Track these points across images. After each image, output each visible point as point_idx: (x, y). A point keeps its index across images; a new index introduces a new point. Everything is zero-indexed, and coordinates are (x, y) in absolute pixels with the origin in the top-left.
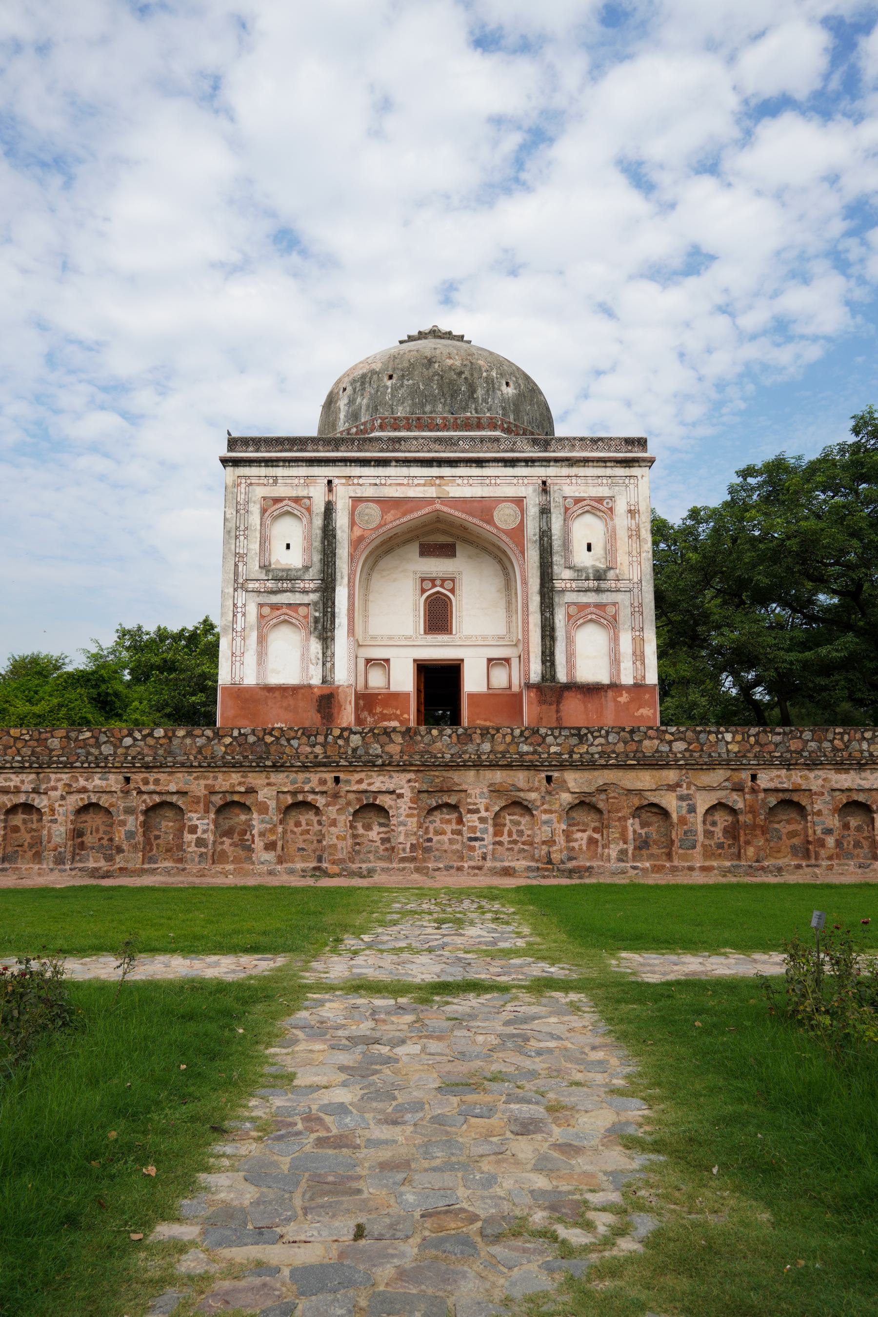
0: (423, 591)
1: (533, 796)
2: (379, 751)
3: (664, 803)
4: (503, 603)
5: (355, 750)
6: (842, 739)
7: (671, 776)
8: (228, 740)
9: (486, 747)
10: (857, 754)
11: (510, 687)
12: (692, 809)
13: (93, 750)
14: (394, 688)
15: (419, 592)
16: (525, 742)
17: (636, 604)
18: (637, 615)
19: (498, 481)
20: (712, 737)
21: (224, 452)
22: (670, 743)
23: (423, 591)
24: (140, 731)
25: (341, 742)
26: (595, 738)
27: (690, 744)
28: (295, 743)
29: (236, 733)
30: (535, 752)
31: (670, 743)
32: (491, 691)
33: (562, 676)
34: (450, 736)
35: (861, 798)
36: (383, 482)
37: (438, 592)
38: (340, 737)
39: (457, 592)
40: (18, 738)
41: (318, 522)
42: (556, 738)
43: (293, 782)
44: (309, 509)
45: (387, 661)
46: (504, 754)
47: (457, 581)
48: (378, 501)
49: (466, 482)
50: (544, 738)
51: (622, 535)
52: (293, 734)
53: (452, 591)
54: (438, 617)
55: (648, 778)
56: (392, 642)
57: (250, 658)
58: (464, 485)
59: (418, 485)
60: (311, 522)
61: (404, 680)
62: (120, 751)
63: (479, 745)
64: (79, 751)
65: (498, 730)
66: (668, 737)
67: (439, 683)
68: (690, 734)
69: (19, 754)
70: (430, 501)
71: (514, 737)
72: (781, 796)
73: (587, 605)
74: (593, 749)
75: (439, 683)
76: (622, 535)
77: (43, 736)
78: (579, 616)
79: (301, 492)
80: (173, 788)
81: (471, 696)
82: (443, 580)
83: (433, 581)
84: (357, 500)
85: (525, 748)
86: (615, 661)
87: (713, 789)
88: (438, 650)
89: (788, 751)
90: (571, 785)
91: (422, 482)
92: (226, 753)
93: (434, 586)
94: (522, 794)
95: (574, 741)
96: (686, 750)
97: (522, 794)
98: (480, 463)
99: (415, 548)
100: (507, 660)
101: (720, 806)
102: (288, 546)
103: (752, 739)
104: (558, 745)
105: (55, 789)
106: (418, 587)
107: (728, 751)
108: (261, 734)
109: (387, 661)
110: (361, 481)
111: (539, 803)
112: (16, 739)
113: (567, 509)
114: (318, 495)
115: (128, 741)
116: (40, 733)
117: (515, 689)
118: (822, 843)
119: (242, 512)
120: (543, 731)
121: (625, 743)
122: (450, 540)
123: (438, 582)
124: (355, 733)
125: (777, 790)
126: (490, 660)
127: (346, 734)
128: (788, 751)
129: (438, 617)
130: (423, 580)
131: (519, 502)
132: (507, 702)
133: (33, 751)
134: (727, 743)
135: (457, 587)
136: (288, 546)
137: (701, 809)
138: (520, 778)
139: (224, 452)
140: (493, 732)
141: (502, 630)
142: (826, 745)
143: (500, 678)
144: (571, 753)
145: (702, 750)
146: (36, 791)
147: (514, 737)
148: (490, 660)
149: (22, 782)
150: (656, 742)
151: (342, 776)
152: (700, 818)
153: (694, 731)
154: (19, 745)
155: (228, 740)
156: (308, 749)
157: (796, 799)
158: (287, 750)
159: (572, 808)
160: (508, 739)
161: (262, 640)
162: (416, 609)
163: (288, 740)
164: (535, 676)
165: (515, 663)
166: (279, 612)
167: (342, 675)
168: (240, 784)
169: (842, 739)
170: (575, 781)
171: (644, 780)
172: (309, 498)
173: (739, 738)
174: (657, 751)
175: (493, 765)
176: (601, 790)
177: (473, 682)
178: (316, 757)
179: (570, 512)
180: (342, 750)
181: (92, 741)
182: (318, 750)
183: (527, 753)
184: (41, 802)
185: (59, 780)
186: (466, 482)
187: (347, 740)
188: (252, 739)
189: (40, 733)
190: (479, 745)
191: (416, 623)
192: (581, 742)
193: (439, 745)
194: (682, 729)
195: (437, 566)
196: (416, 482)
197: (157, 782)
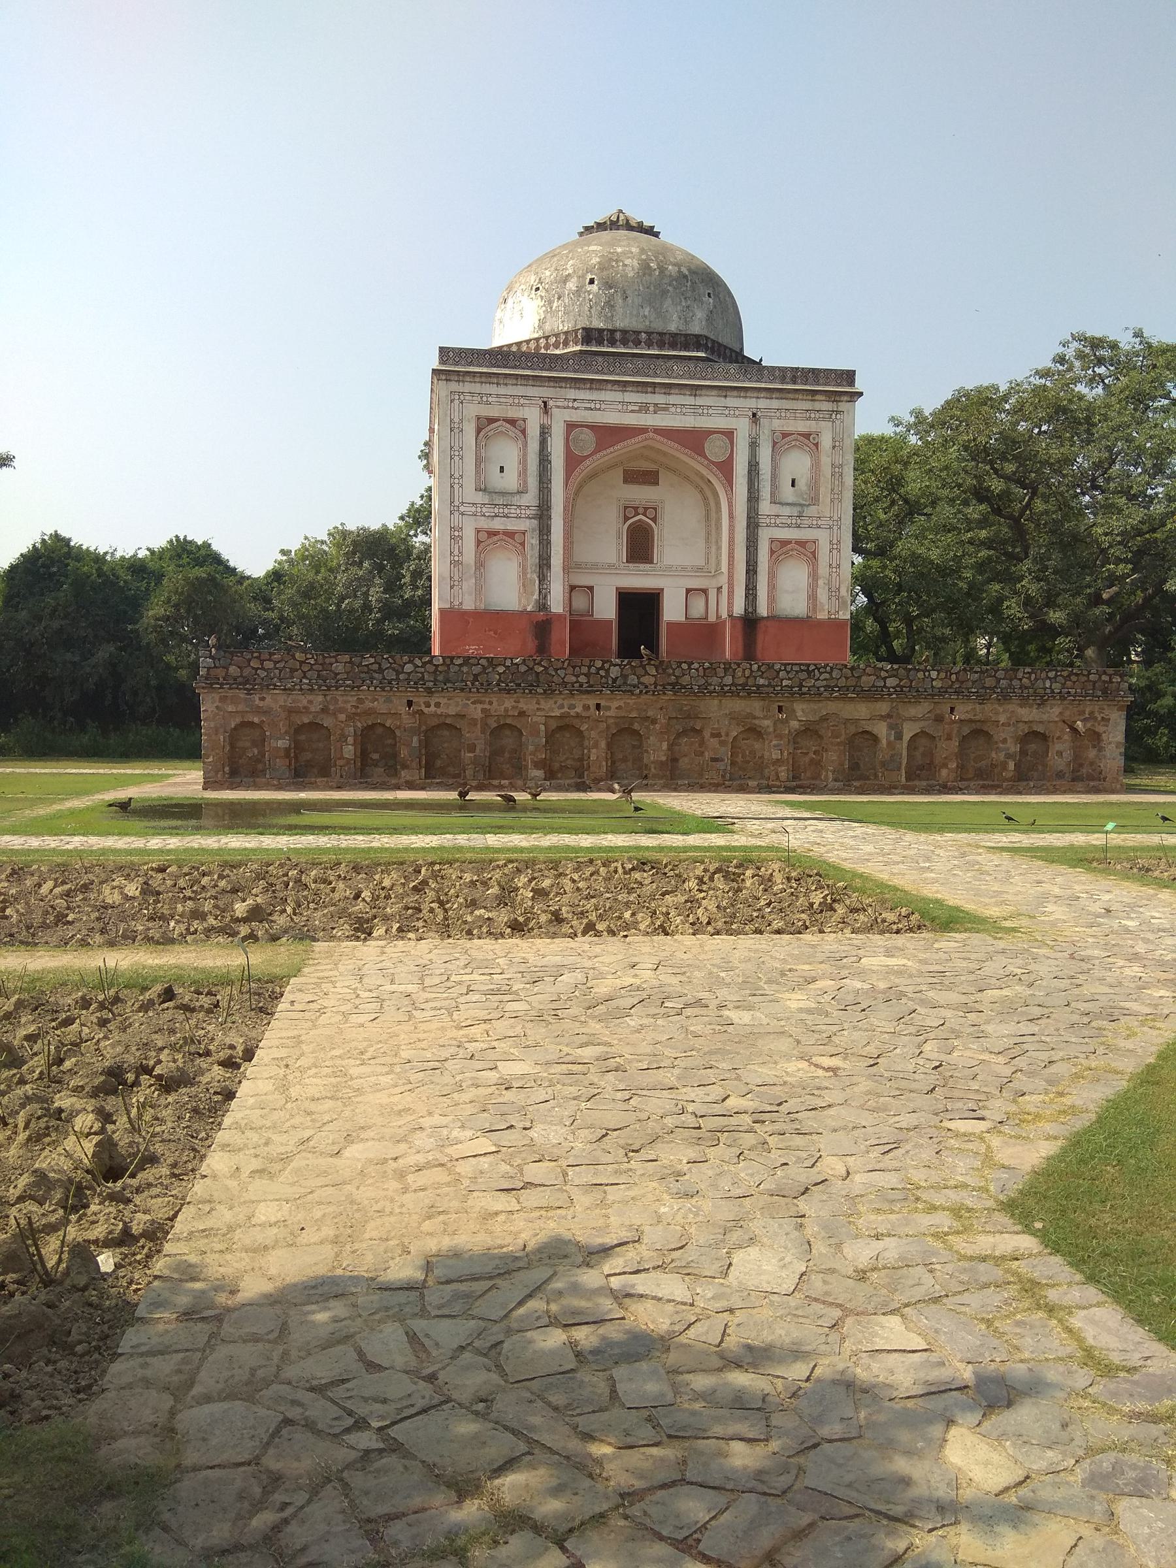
0: (626, 519)
1: (766, 723)
2: (636, 681)
3: (875, 731)
4: (703, 534)
5: (614, 680)
6: (1029, 678)
7: (883, 707)
8: (501, 669)
9: (728, 680)
10: (1042, 691)
11: (706, 618)
12: (899, 737)
13: (376, 675)
14: (598, 615)
15: (622, 519)
16: (761, 677)
17: (835, 541)
18: (835, 552)
19: (711, 411)
20: (920, 675)
21: (435, 364)
22: (884, 679)
23: (626, 519)
24: (420, 658)
25: (602, 673)
26: (821, 673)
27: (901, 680)
28: (561, 673)
29: (508, 663)
30: (769, 685)
31: (884, 679)
32: (689, 621)
33: (763, 611)
34: (697, 670)
35: (1040, 729)
36: (598, 406)
37: (640, 520)
38: (602, 668)
39: (659, 521)
40: (304, 662)
41: (534, 446)
42: (788, 672)
43: (562, 706)
44: (524, 432)
45: (591, 588)
46: (744, 685)
47: (659, 511)
48: (593, 428)
49: (679, 410)
50: (778, 673)
51: (827, 470)
52: (560, 665)
53: (654, 520)
54: (640, 547)
55: (864, 709)
56: (594, 567)
57: (469, 584)
58: (676, 414)
59: (632, 411)
60: (525, 445)
61: (606, 608)
62: (402, 677)
63: (722, 678)
64: (363, 675)
65: (739, 665)
66: (883, 674)
67: (640, 608)
68: (902, 672)
69: (305, 677)
70: (643, 430)
71: (752, 671)
72: (974, 726)
73: (788, 542)
74: (818, 683)
75: (640, 608)
76: (827, 470)
77: (328, 661)
78: (780, 552)
79: (512, 413)
80: (452, 711)
81: (669, 624)
82: (646, 509)
83: (636, 509)
84: (571, 426)
85: (761, 681)
86: (813, 597)
87: (919, 719)
88: (639, 580)
89: (984, 687)
90: (799, 713)
91: (637, 408)
92: (500, 680)
93: (637, 514)
94: (757, 722)
95: (803, 675)
96: (898, 686)
97: (757, 722)
98: (695, 390)
99: (618, 474)
100: (705, 591)
101: (923, 733)
102: (502, 469)
103: (954, 677)
104: (790, 679)
105: (342, 710)
106: (622, 515)
107: (932, 687)
108: (531, 664)
109: (591, 588)
110: (576, 405)
111: (771, 729)
112: (302, 663)
113: (775, 444)
114: (533, 417)
115: (409, 668)
116: (325, 657)
117: (712, 618)
118: (1004, 766)
119: (456, 431)
120: (777, 667)
121: (847, 678)
122: (652, 467)
123: (641, 510)
124: (615, 665)
125: (971, 721)
126: (688, 591)
127: (607, 666)
128: (984, 687)
129: (640, 547)
130: (626, 508)
131: (729, 434)
132: (703, 633)
133: (319, 676)
134: (933, 680)
135: (659, 516)
136: (502, 469)
137: (907, 737)
138: (755, 706)
139: (435, 364)
140: (734, 666)
141: (702, 562)
142: (1015, 683)
143: (697, 609)
144: (801, 686)
145: (911, 686)
146: (324, 710)
147: (752, 671)
148: (688, 591)
149: (310, 702)
150: (873, 678)
151: (603, 703)
152: (905, 745)
153: (905, 669)
154: (305, 668)
155: (501, 669)
156: (574, 679)
157: (985, 729)
158: (555, 679)
159: (799, 733)
160: (747, 673)
161: (480, 564)
162: (619, 537)
163: (556, 670)
164: (739, 609)
165: (712, 594)
166: (496, 538)
167: (557, 605)
168: (513, 707)
169: (1029, 678)
170: (803, 711)
171: (860, 710)
172: (524, 420)
173: (943, 675)
174: (873, 686)
175: (735, 694)
176: (824, 719)
177: (672, 611)
178: (581, 686)
179: (778, 446)
180: (604, 680)
181: (376, 667)
182: (583, 679)
183: (763, 686)
184: (327, 722)
185: (346, 702)
186: (679, 410)
187: (607, 671)
188: (523, 668)
189: (325, 657)
190: (722, 678)
191: (619, 551)
192: (809, 677)
193: (687, 677)
194: (895, 666)
195: (641, 494)
196: (630, 408)
197: (438, 705)
